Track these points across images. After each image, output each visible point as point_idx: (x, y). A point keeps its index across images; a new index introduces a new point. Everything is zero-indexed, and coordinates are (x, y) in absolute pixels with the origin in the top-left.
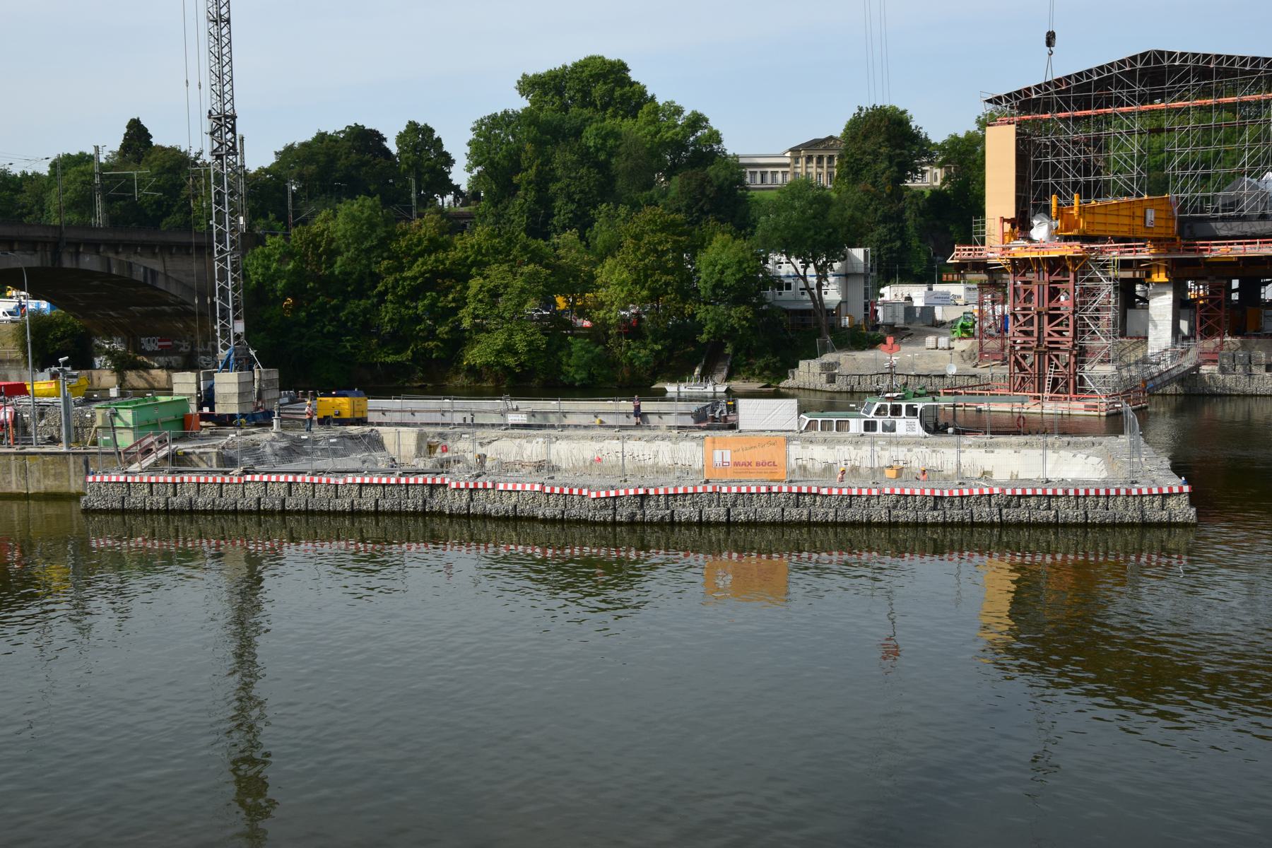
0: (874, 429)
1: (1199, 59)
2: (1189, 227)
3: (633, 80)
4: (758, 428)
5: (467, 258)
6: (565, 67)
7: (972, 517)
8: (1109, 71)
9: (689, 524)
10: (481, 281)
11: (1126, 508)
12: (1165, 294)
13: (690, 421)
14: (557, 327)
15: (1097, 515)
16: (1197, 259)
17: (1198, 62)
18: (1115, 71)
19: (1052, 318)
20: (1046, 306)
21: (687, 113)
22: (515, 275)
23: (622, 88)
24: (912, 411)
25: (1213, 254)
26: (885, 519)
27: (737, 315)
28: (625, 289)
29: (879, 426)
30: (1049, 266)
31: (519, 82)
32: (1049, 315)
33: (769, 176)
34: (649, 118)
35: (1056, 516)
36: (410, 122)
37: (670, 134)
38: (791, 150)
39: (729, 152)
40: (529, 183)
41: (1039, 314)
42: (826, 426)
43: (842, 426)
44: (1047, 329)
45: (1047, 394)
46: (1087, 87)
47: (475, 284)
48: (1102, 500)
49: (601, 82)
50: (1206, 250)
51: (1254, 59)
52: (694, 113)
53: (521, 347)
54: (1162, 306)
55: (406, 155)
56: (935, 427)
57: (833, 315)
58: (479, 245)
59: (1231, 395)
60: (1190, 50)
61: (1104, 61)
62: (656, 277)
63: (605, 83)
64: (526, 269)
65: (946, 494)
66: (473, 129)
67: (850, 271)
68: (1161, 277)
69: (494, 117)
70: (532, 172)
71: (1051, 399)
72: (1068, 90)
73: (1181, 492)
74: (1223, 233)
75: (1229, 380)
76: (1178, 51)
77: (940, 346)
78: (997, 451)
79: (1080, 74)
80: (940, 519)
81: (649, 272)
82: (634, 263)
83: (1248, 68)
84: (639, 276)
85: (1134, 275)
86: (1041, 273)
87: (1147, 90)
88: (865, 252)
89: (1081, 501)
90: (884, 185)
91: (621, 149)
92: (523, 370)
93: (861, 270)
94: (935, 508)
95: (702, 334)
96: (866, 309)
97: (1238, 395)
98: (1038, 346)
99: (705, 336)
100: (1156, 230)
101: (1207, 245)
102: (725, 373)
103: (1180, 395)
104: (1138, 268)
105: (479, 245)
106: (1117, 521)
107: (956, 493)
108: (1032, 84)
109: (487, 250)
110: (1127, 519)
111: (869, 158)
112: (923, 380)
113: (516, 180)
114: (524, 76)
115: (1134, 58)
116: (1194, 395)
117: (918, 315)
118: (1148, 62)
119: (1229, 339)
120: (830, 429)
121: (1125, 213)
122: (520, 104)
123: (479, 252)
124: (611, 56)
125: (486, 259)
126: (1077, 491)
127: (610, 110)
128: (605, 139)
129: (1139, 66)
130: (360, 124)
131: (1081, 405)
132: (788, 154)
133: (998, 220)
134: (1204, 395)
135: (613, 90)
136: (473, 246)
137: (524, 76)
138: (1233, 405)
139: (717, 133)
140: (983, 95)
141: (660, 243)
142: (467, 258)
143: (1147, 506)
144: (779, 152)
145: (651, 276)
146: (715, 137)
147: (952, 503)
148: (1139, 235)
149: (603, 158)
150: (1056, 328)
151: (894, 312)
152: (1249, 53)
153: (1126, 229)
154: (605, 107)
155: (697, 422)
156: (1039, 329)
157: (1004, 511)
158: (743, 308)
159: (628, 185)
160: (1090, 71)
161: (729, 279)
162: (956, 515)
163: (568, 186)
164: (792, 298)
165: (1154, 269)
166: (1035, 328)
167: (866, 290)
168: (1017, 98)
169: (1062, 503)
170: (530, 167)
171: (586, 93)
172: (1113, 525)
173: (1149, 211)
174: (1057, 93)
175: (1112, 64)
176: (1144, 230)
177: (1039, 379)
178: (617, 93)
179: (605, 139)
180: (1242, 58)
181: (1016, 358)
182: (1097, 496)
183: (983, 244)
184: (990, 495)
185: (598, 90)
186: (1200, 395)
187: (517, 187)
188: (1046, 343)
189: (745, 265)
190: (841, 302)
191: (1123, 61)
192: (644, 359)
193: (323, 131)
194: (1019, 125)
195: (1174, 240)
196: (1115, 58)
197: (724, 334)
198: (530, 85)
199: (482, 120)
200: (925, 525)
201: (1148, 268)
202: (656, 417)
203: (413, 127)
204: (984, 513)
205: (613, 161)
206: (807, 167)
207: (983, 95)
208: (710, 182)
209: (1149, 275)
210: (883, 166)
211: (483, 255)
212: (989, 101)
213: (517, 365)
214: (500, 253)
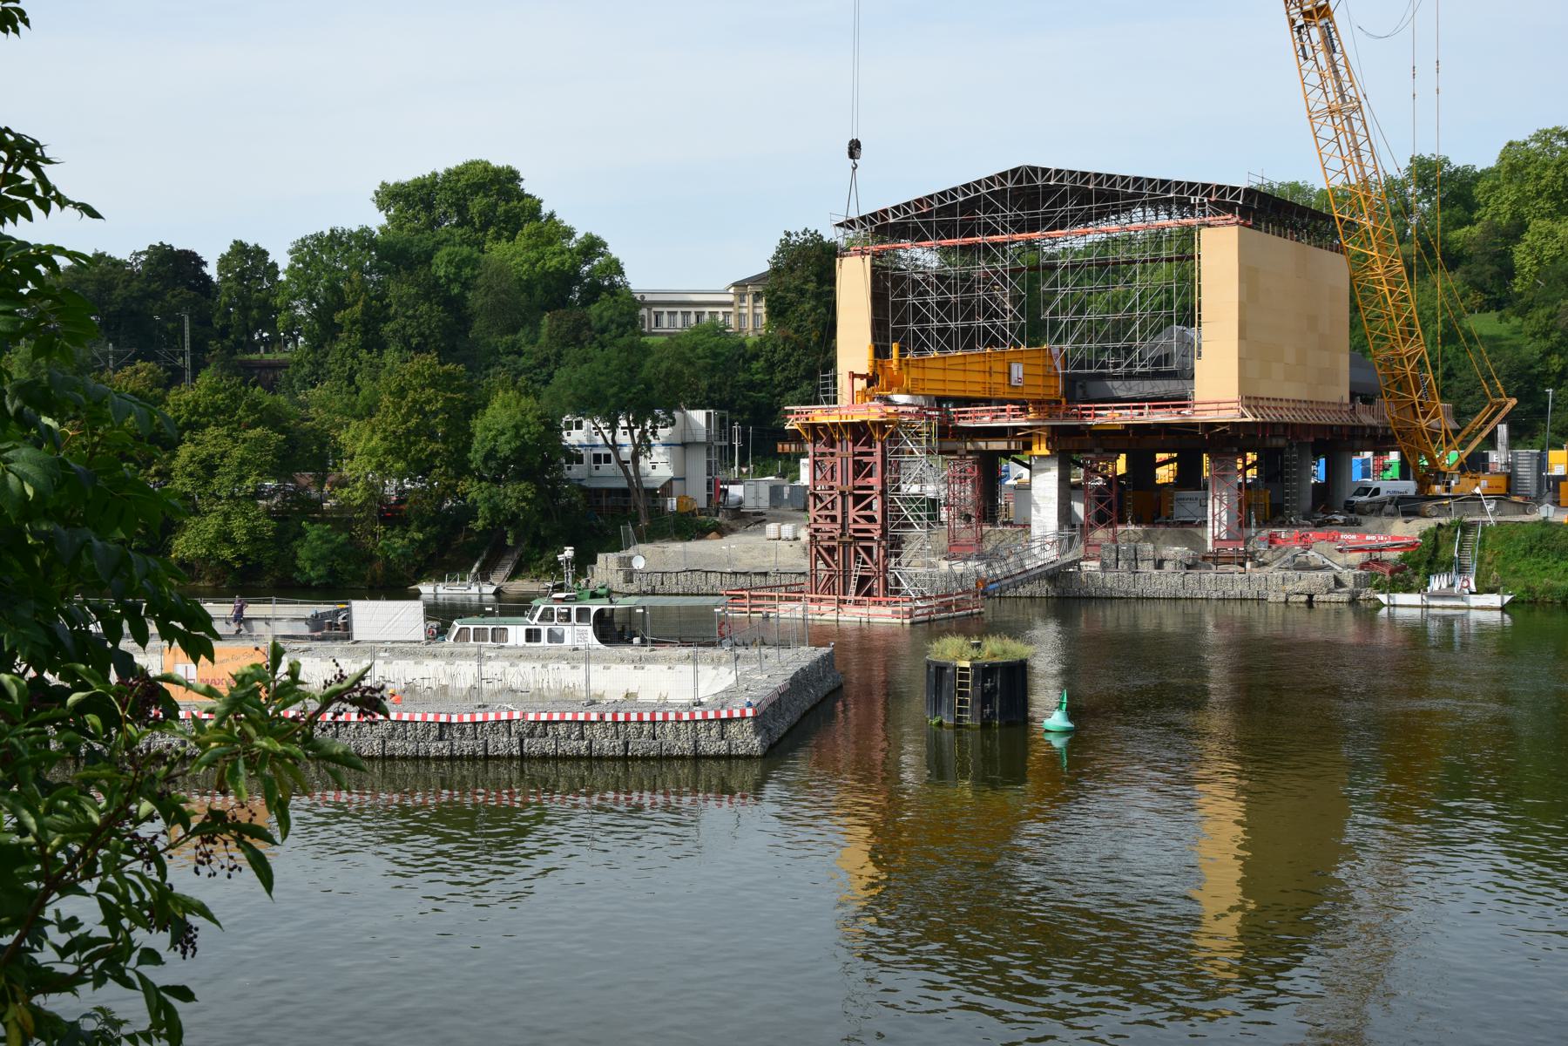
0: (538, 639)
1: (1128, 183)
3: (526, 192)
4: (376, 639)
5: (179, 418)
6: (435, 175)
7: (486, 750)
8: (976, 190)
9: (717, 757)
10: (192, 448)
11: (677, 737)
12: (1049, 470)
13: (304, 629)
14: (301, 509)
15: (638, 747)
16: (1078, 426)
17: (1075, 182)
19: (858, 500)
20: (850, 484)
21: (579, 236)
22: (235, 441)
23: (508, 202)
24: (583, 615)
25: (1098, 421)
26: (377, 751)
27: (513, 494)
28: (374, 460)
29: (544, 635)
30: (853, 434)
31: (377, 193)
32: (855, 496)
33: (665, 318)
34: (530, 242)
35: (589, 747)
36: (235, 242)
37: (554, 263)
38: (735, 285)
39: (633, 287)
40: (354, 323)
41: (842, 493)
42: (480, 635)
43: (499, 635)
44: (852, 513)
45: (851, 597)
46: (950, 210)
47: (185, 451)
48: (646, 727)
49: (481, 194)
50: (1089, 415)
51: (1137, 179)
52: (589, 236)
53: (240, 535)
54: (1046, 485)
55: (228, 284)
56: (612, 630)
57: (657, 495)
58: (197, 403)
60: (1066, 166)
61: (970, 178)
62: (422, 445)
63: (486, 196)
64: (252, 433)
65: (455, 719)
66: (291, 252)
67: (689, 439)
68: (1040, 449)
69: (318, 238)
70: (358, 308)
71: (857, 603)
72: (929, 214)
73: (743, 718)
74: (1122, 394)
75: (1110, 579)
76: (1053, 166)
77: (783, 536)
78: (648, 667)
79: (943, 193)
80: (446, 752)
81: (412, 438)
82: (392, 428)
84: (400, 444)
85: (1009, 445)
88: (708, 415)
89: (621, 727)
91: (480, 281)
92: (245, 566)
93: (702, 438)
94: (440, 738)
95: (476, 520)
96: (709, 488)
98: (842, 535)
99: (480, 523)
100: (1027, 390)
101: (966, 412)
102: (507, 570)
104: (1014, 436)
105: (197, 403)
106: (664, 754)
107: (467, 718)
108: (889, 205)
109: (206, 409)
110: (676, 752)
113: (337, 318)
114: (384, 185)
115: (1004, 175)
117: (786, 497)
118: (1020, 181)
119: (1132, 527)
120: (538, 639)
121: (976, 367)
122: (376, 220)
123: (194, 411)
124: (497, 162)
125: (204, 420)
126: (640, 715)
127: (491, 231)
128: (459, 267)
129: (1009, 185)
130: (166, 243)
135: (496, 205)
136: (187, 404)
137: (384, 185)
139: (616, 261)
140: (834, 217)
141: (429, 401)
142: (179, 418)
143: (703, 735)
144: (722, 287)
145: (415, 443)
146: (615, 267)
147: (463, 731)
148: (1000, 395)
149: (456, 291)
150: (862, 513)
151: (757, 492)
152: (1132, 171)
153: (978, 388)
154: (484, 227)
155: (312, 631)
156: (843, 513)
157: (526, 741)
158: (523, 486)
159: (488, 327)
161: (505, 450)
162: (466, 746)
163: (404, 327)
164: (612, 473)
165: (1035, 439)
166: (838, 512)
167: (709, 463)
168: (872, 223)
169: (597, 730)
170: (356, 302)
171: (462, 209)
172: (660, 758)
173: (1014, 367)
176: (1007, 389)
178: (501, 208)
179: (459, 267)
180: (1124, 178)
181: (818, 551)
182: (641, 721)
184: (509, 721)
185: (477, 204)
186: (1074, 598)
187: (340, 327)
189: (524, 431)
190: (671, 480)
191: (991, 179)
192: (400, 551)
193: (100, 251)
195: (1058, 402)
196: (982, 175)
197: (502, 521)
198: (391, 196)
199: (303, 240)
200: (427, 758)
201: (1026, 439)
202: (262, 624)
203: (240, 249)
204: (502, 744)
205: (469, 295)
206: (754, 307)
207: (834, 217)
208: (588, 324)
209: (1028, 446)
211: (201, 415)
213: (235, 559)
214: (222, 412)
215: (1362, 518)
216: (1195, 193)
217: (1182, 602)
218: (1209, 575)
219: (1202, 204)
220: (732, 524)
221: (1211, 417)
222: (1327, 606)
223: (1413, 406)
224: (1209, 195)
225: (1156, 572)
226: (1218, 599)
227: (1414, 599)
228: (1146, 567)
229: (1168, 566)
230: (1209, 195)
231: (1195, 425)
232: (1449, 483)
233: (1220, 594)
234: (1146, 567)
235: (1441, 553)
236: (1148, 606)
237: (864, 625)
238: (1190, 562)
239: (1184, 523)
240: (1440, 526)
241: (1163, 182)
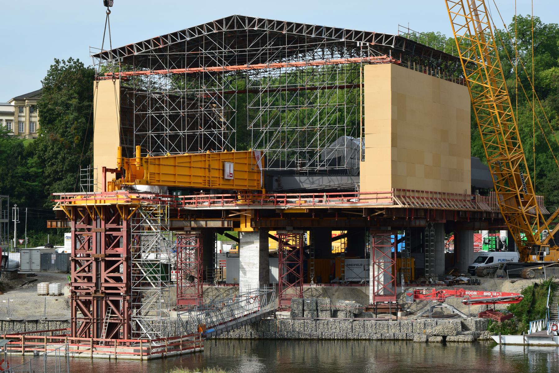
2: (277, 180)
8: (200, 33)
12: (253, 243)
16: (274, 210)
17: (273, 28)
18: (205, 33)
19: (109, 264)
20: (103, 253)
25: (289, 206)
30: (105, 214)
38: (15, 99)
41: (96, 260)
44: (104, 275)
45: (103, 339)
46: (180, 47)
50: (283, 202)
51: (318, 28)
59: (299, 340)
60: (266, 16)
61: (195, 24)
68: (246, 227)
72: (164, 49)
74: (307, 186)
75: (298, 324)
76: (257, 16)
77: (51, 292)
79: (175, 34)
83: (313, 36)
85: (223, 224)
86: (98, 221)
87: (236, 52)
90: (73, 136)
97: (306, 340)
98: (96, 292)
103: (254, 339)
104: (227, 217)
108: (134, 42)
111: (59, 108)
112: (18, 326)
115: (220, 22)
116: (267, 339)
117: (53, 262)
118: (232, 27)
119: (314, 286)
129: (224, 29)
131: (131, 350)
132: (13, 103)
133: (100, 170)
134: (276, 339)
138: (302, 348)
140: (92, 50)
150: (112, 275)
151: (30, 259)
153: (200, 180)
160: (184, 32)
165: (242, 220)
166: (93, 274)
168: (121, 55)
173: (227, 165)
174: (156, 51)
175: (201, 27)
176: (222, 182)
177: (97, 324)
180: (308, 26)
183: (92, 190)
186: (272, 339)
188: (103, 289)
191: (211, 24)
194: (124, 80)
195: (260, 192)
196: (204, 21)
206: (30, 117)
207: (92, 50)
210: (71, 117)
212: (97, 56)
215: (481, 280)
216: (360, 39)
217: (351, 343)
218: (371, 322)
219: (365, 47)
220: (11, 283)
221: (373, 204)
222: (456, 344)
223: (516, 197)
224: (370, 40)
225: (331, 319)
226: (378, 340)
227: (518, 339)
228: (325, 316)
229: (341, 315)
230: (370, 40)
231: (360, 210)
232: (542, 254)
233: (379, 336)
234: (325, 316)
235: (537, 305)
236: (326, 345)
237: (112, 361)
238: (357, 312)
239: (352, 283)
240: (536, 285)
241: (337, 30)
